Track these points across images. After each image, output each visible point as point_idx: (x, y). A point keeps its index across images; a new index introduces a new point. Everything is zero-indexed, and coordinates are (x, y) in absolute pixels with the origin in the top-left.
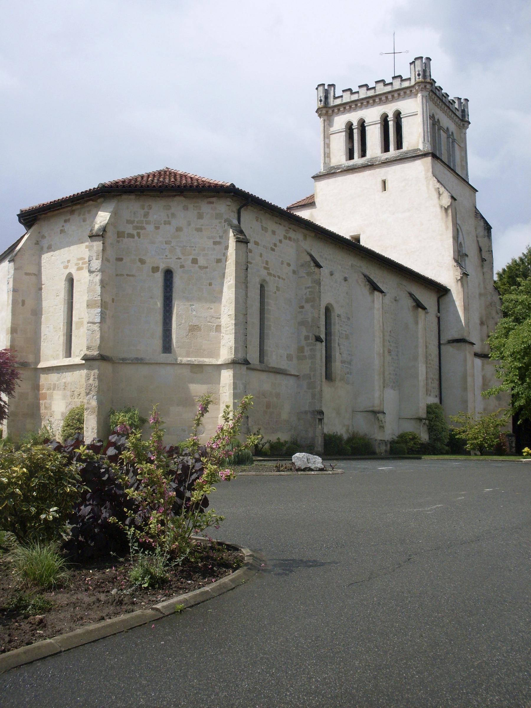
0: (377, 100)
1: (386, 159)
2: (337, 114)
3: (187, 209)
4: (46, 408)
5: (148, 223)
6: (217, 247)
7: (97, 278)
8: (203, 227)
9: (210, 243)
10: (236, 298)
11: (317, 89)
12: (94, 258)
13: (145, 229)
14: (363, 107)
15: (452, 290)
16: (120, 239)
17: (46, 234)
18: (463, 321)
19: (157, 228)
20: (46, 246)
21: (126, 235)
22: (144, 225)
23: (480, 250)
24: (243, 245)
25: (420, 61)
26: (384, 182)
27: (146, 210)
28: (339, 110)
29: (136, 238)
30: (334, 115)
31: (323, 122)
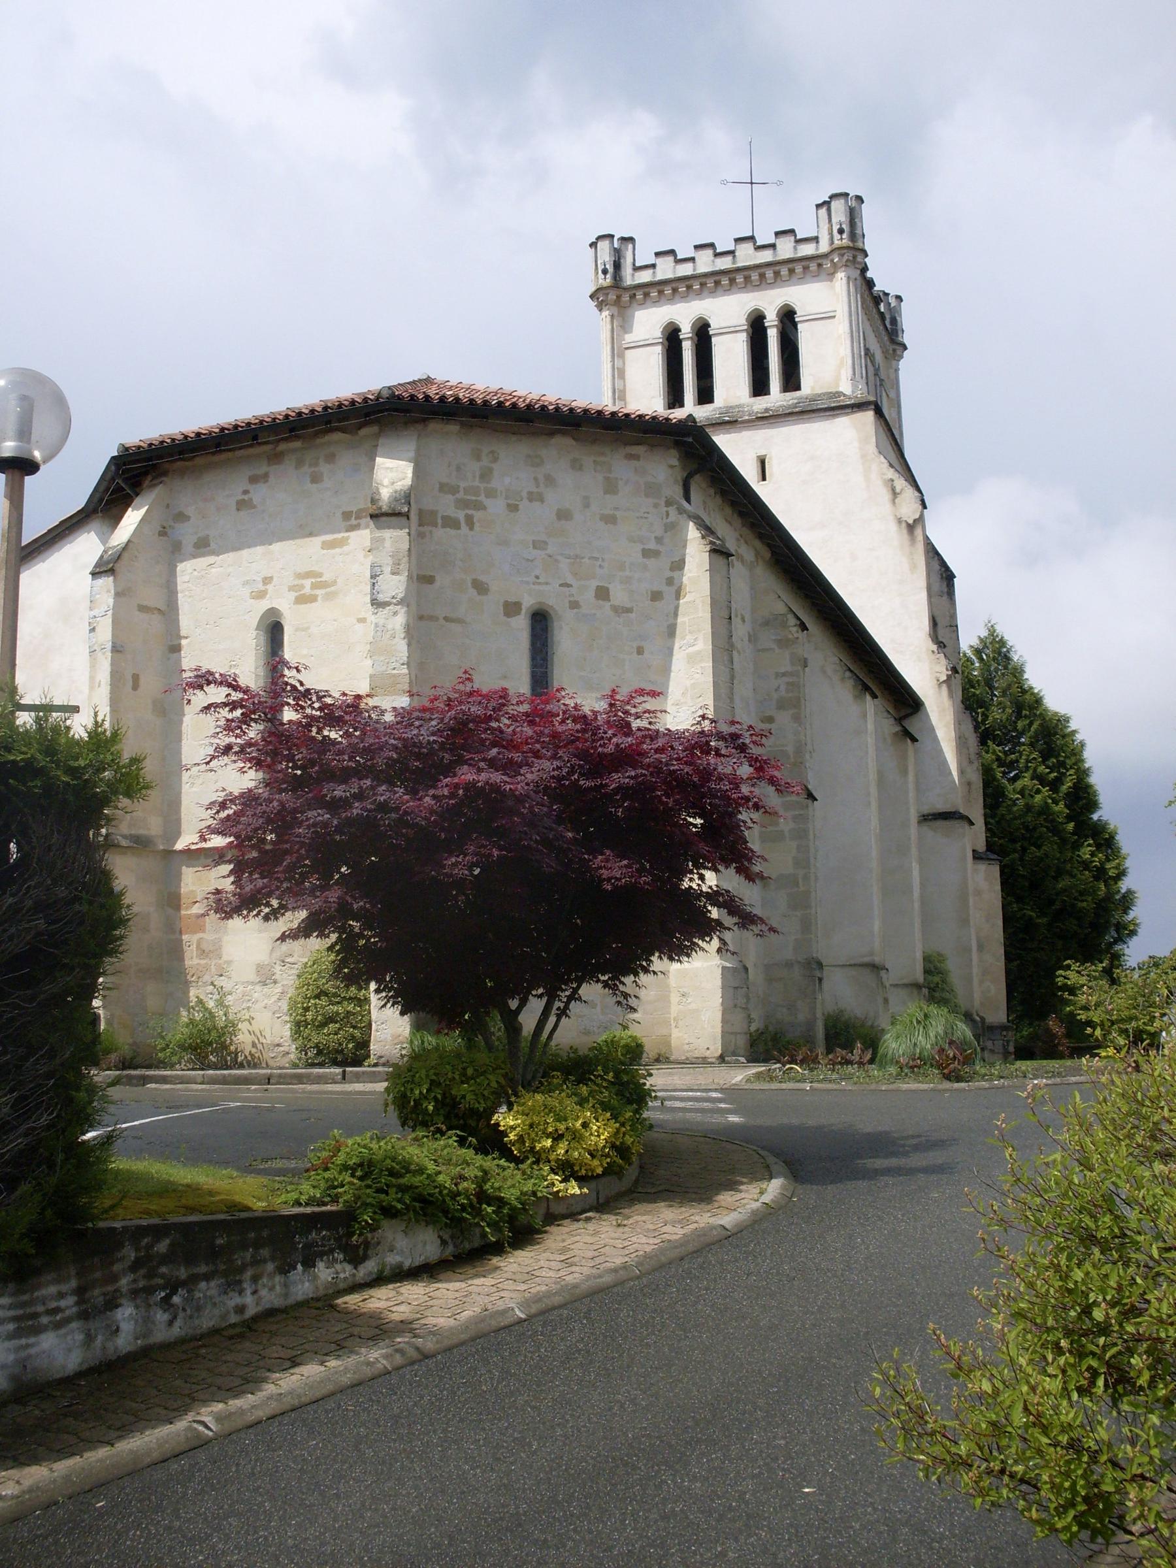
0: (740, 279)
1: (767, 410)
2: (642, 304)
3: (581, 468)
4: (203, 953)
5: (491, 494)
6: (651, 563)
7: (398, 621)
8: (618, 513)
9: (637, 556)
10: (715, 684)
11: (593, 245)
12: (387, 570)
13: (485, 508)
14: (706, 292)
15: (927, 704)
16: (426, 529)
17: (190, 511)
18: (955, 773)
19: (513, 508)
20: (188, 542)
21: (440, 521)
22: (482, 498)
24: (721, 561)
25: (842, 201)
27: (485, 461)
28: (646, 295)
29: (464, 528)
30: (635, 305)
31: (609, 318)
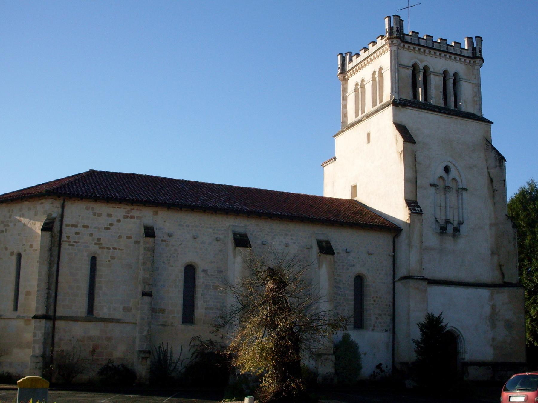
23: (492, 181)
26: (369, 135)
